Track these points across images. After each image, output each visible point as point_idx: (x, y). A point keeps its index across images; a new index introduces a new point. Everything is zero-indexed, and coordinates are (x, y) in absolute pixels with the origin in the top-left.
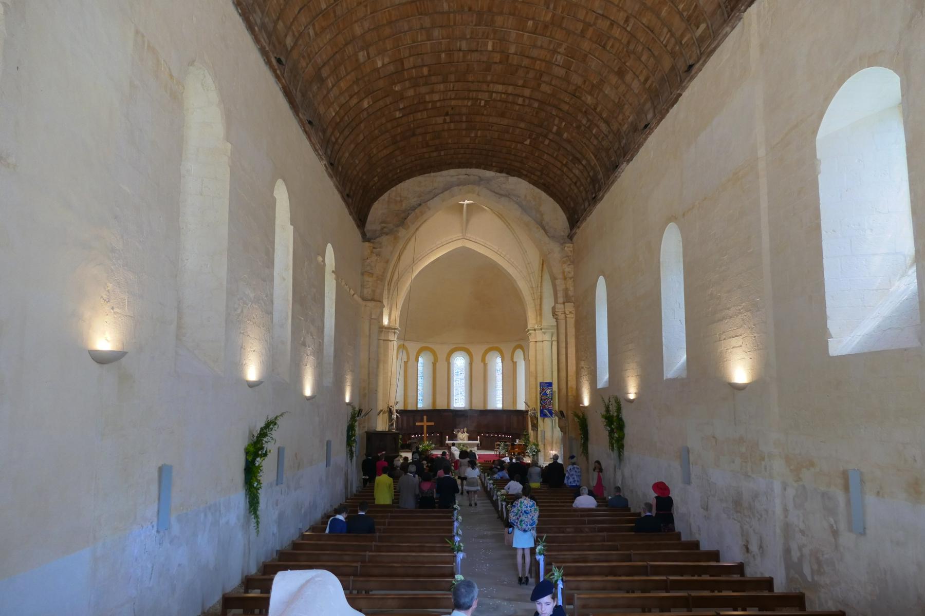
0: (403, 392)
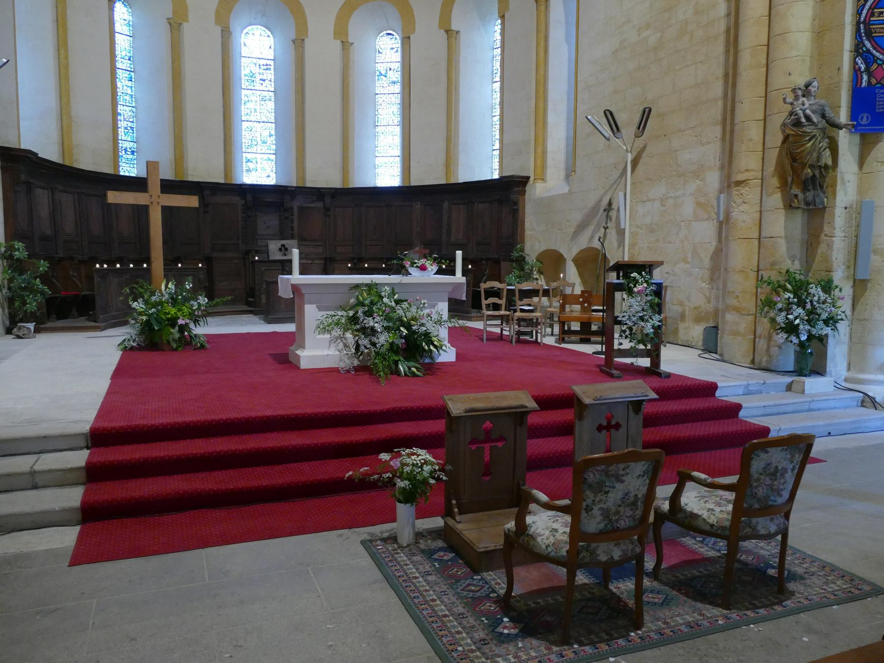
0: (51, 100)
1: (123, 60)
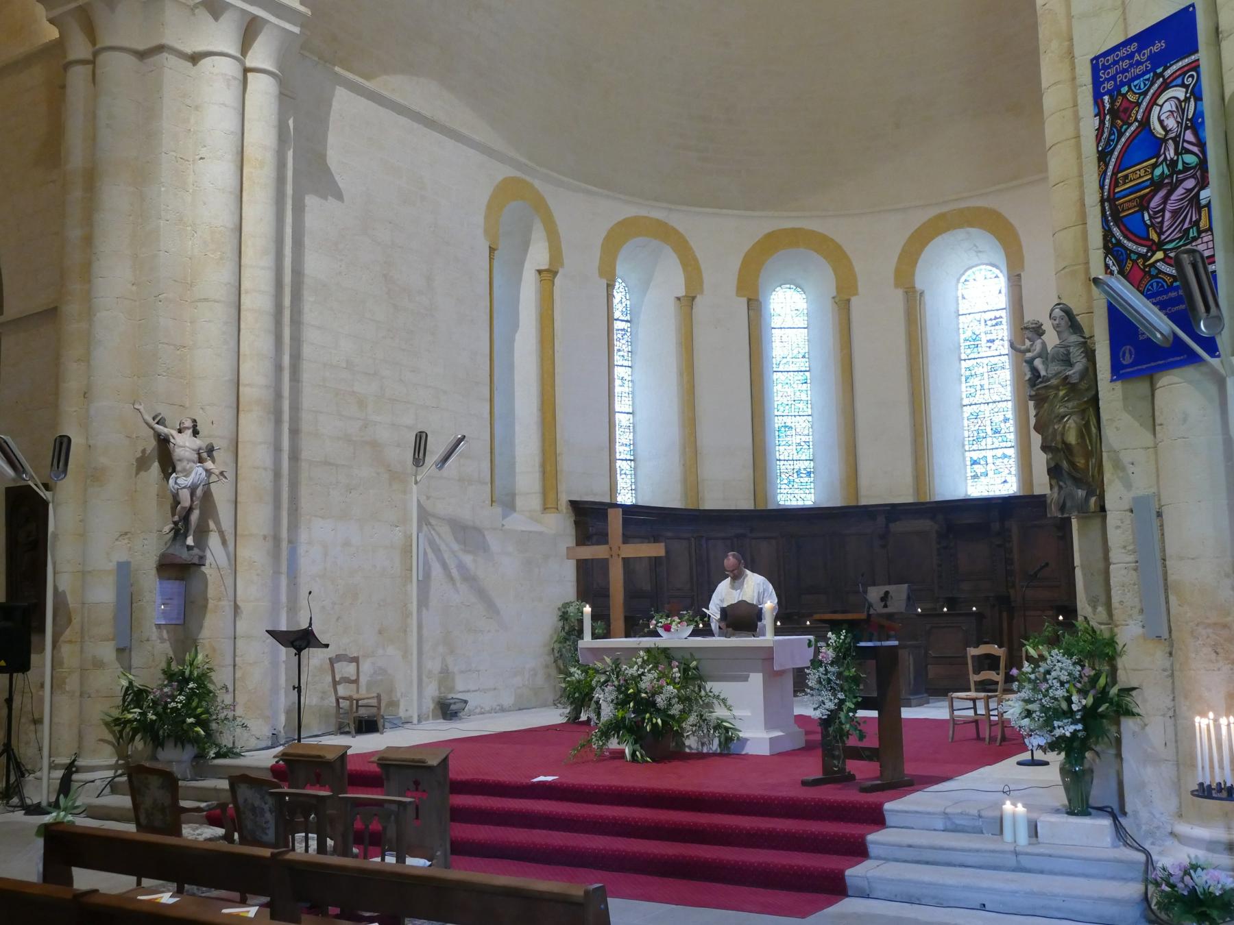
1: (794, 360)
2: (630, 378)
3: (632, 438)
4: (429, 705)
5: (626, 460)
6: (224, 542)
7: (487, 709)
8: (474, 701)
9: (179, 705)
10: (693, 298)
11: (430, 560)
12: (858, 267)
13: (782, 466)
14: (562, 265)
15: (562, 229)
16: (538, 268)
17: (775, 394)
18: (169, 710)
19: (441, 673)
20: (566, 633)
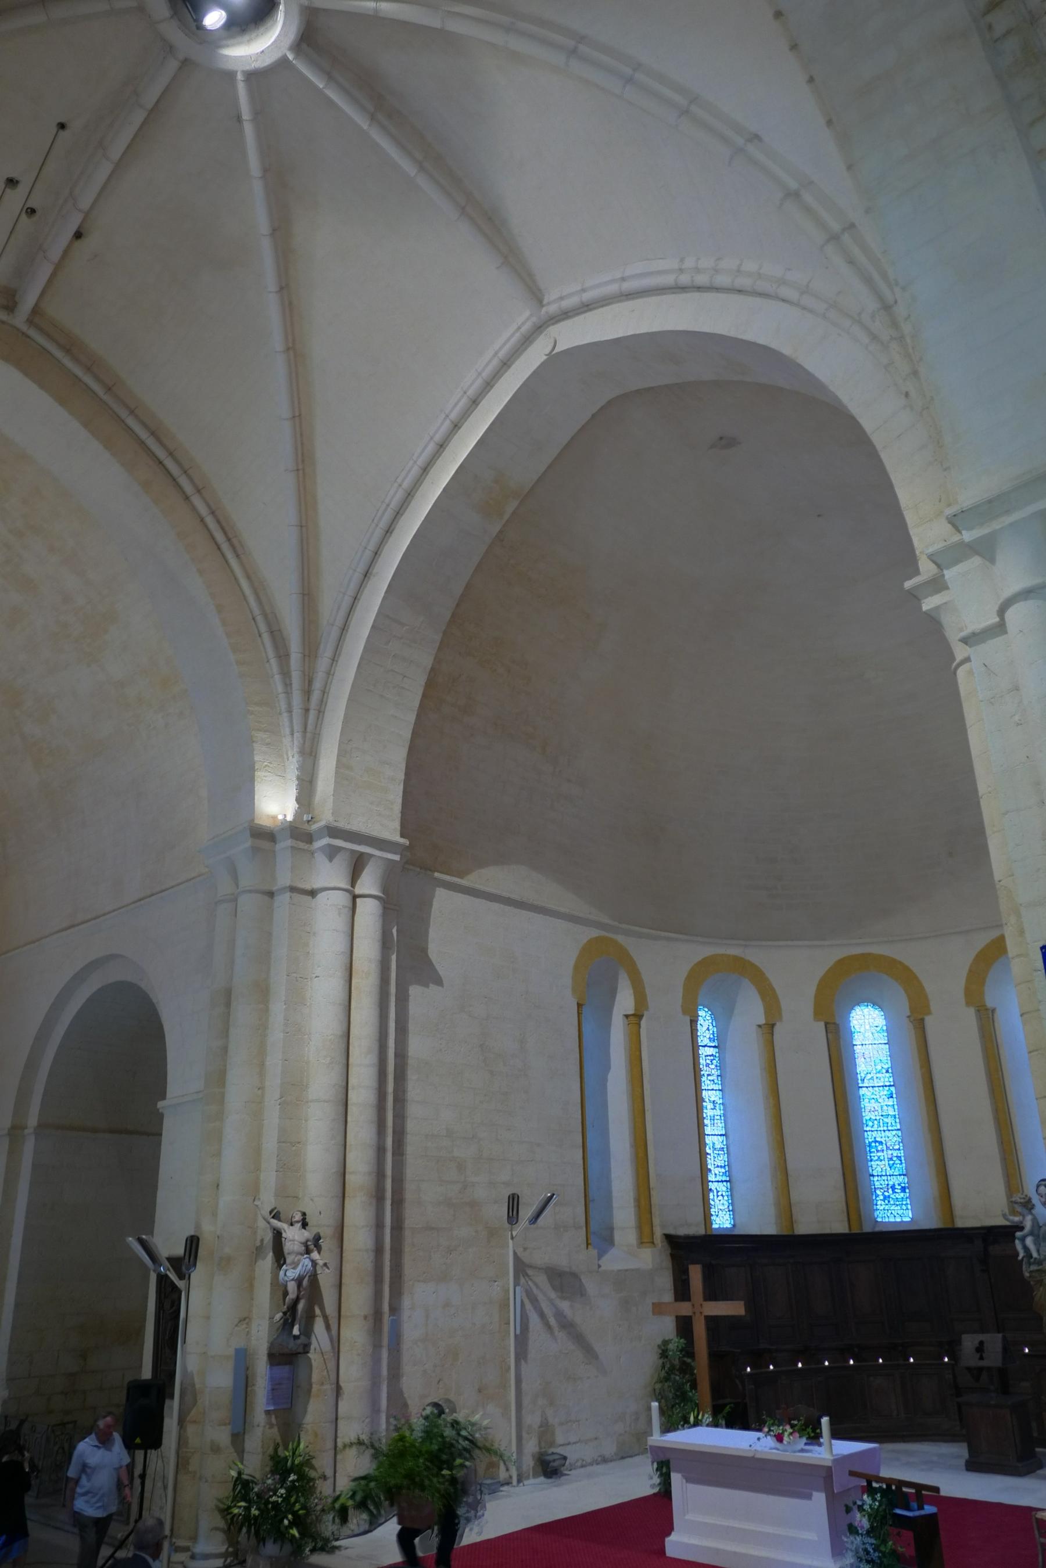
1: (878, 1075)
2: (721, 1101)
3: (726, 1160)
4: (528, 1462)
5: (722, 1181)
6: (328, 1327)
7: (589, 1461)
8: (572, 1454)
9: (280, 1500)
10: (773, 1026)
11: (528, 1312)
12: (929, 987)
13: (877, 1182)
14: (647, 1009)
15: (646, 977)
16: (625, 1014)
17: (863, 1110)
18: (270, 1506)
19: (541, 1426)
20: (667, 1373)
